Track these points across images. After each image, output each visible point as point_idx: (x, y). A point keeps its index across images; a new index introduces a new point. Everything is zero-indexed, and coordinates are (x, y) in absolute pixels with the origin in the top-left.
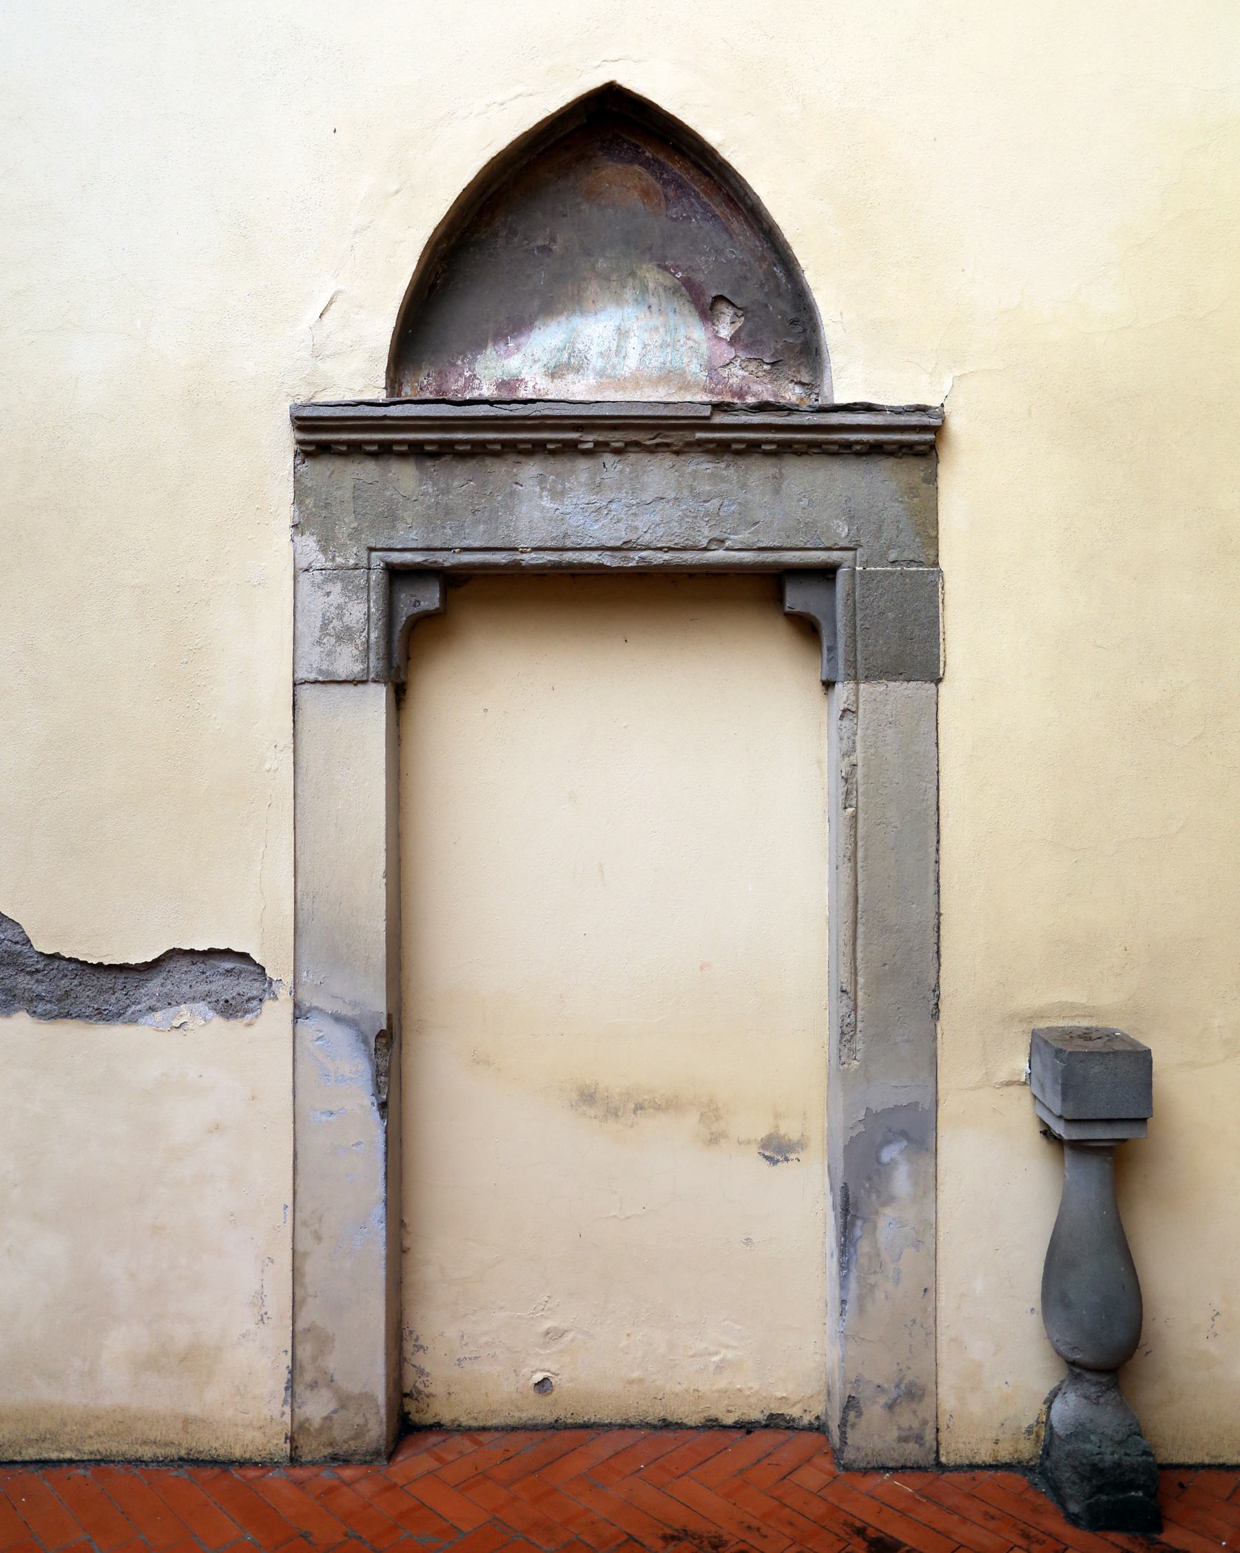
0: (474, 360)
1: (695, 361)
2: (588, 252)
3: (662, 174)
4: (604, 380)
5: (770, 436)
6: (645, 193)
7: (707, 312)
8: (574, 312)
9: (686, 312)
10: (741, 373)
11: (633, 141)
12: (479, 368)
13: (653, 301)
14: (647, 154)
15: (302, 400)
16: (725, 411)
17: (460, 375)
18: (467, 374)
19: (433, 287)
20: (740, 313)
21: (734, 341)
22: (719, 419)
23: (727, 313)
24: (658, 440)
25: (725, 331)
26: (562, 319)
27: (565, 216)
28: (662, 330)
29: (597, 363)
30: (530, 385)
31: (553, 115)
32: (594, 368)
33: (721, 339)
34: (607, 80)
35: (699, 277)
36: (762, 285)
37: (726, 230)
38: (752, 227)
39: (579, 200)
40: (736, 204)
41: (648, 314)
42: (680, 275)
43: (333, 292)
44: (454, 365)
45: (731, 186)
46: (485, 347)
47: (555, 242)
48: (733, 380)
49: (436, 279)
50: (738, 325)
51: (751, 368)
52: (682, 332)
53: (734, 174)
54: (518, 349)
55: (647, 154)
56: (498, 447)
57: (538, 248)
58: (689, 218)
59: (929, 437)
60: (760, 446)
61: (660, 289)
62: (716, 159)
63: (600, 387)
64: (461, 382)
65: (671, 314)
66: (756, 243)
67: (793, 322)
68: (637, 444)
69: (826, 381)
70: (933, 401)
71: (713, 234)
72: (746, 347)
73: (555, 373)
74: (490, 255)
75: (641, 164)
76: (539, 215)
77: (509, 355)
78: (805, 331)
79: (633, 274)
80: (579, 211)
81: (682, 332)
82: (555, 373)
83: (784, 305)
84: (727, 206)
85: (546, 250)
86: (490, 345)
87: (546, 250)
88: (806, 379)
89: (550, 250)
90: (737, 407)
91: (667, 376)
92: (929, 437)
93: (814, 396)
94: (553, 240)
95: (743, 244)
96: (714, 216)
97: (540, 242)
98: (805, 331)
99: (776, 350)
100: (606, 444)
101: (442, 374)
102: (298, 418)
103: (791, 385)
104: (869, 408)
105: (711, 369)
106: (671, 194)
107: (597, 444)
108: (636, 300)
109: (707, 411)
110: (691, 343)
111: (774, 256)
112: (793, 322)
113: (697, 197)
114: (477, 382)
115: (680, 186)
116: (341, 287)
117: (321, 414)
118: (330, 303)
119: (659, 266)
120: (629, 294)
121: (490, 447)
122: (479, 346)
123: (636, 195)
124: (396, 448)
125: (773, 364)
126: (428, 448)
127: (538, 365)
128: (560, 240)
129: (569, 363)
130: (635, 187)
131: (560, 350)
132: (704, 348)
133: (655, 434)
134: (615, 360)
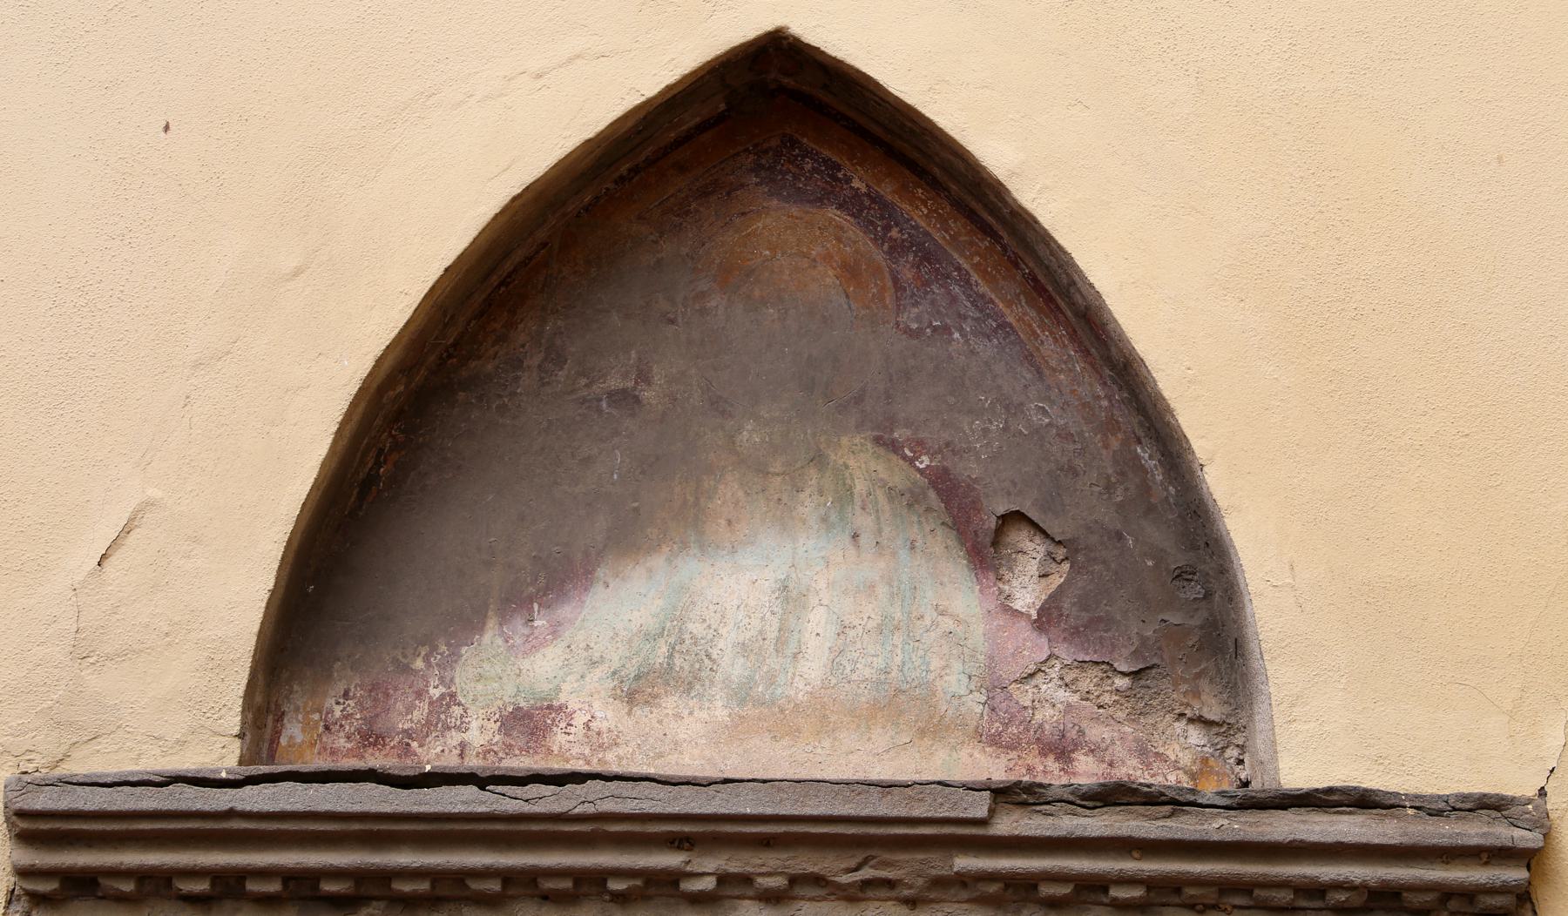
0: (455, 656)
1: (957, 666)
2: (718, 406)
3: (887, 228)
4: (749, 710)
5: (1129, 866)
6: (851, 272)
7: (986, 550)
8: (685, 545)
9: (938, 549)
10: (1062, 695)
11: (826, 153)
12: (463, 678)
13: (864, 522)
14: (856, 184)
15: (38, 764)
16: (1024, 804)
17: (419, 695)
18: (435, 693)
19: (369, 482)
20: (1061, 552)
21: (1045, 619)
22: (1009, 824)
23: (1030, 553)
24: (867, 873)
25: (1027, 594)
26: (658, 561)
27: (672, 322)
28: (882, 590)
29: (734, 668)
30: (580, 720)
31: (649, 101)
32: (727, 681)
33: (1017, 614)
34: (768, 26)
35: (968, 469)
36: (1109, 488)
37: (1029, 358)
38: (1086, 353)
39: (703, 286)
40: (1050, 299)
41: (852, 551)
42: (924, 462)
43: (134, 504)
44: (406, 669)
45: (1039, 260)
46: (481, 629)
47: (648, 382)
48: (1045, 715)
49: (378, 464)
50: (1057, 581)
51: (1085, 685)
52: (929, 595)
53: (1046, 238)
54: (555, 631)
55: (856, 184)
56: (495, 886)
57: (610, 394)
58: (946, 329)
59: (1514, 875)
60: (1105, 890)
61: (881, 496)
62: (1005, 203)
63: (737, 729)
64: (420, 712)
65: (903, 554)
66: (1092, 388)
67: (1182, 575)
68: (817, 880)
69: (1260, 724)
70: (1517, 783)
71: (999, 368)
72: (1075, 634)
73: (636, 691)
74: (502, 409)
75: (840, 207)
76: (615, 319)
77: (533, 645)
78: (1208, 596)
79: (818, 459)
80: (703, 312)
81: (929, 595)
82: (636, 691)
83: (1159, 535)
84: (1031, 303)
85: (626, 399)
86: (492, 623)
87: (626, 399)
88: (1213, 714)
89: (637, 400)
90: (1051, 794)
91: (898, 703)
92: (1514, 875)
93: (1232, 753)
94: (644, 377)
95: (1062, 395)
96: (1004, 325)
97: (615, 383)
98: (1208, 596)
99: (1144, 641)
100: (746, 880)
101: (379, 693)
102: (22, 814)
103: (1180, 726)
104: (1363, 801)
105: (994, 688)
106: (907, 274)
107: (723, 879)
108: (824, 519)
109: (978, 807)
110: (947, 624)
111: (1135, 420)
112: (1182, 575)
113: (966, 282)
114: (457, 711)
115: (928, 257)
116: (153, 492)
117: (80, 805)
118: (127, 530)
119: (878, 441)
120: (808, 506)
121: (475, 885)
122: (468, 625)
123: (830, 276)
124: (253, 886)
125: (1135, 675)
126: (329, 887)
127: (598, 672)
128: (658, 376)
129: (670, 666)
130: (828, 258)
131: (652, 637)
132: (977, 634)
133: (859, 859)
134: (773, 662)
